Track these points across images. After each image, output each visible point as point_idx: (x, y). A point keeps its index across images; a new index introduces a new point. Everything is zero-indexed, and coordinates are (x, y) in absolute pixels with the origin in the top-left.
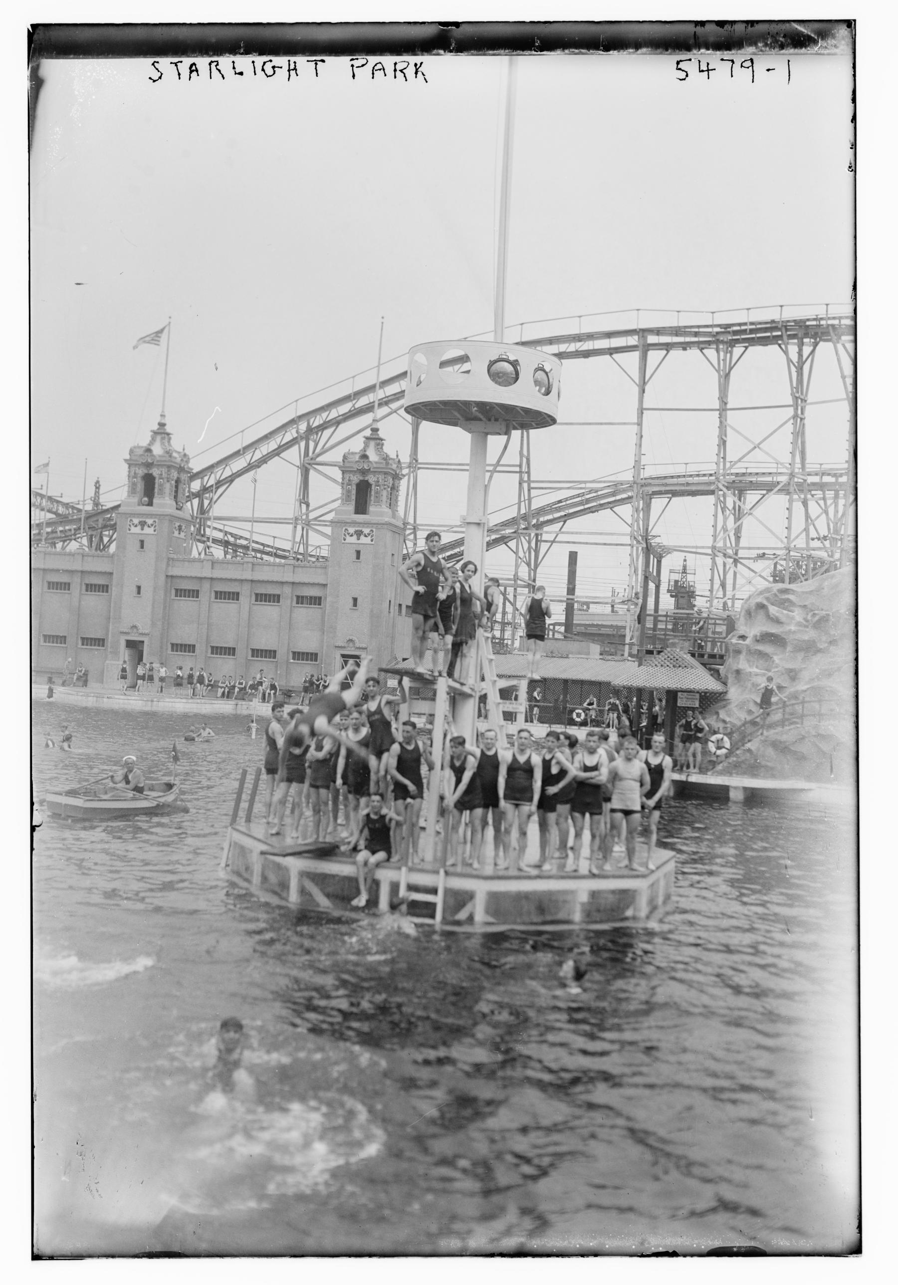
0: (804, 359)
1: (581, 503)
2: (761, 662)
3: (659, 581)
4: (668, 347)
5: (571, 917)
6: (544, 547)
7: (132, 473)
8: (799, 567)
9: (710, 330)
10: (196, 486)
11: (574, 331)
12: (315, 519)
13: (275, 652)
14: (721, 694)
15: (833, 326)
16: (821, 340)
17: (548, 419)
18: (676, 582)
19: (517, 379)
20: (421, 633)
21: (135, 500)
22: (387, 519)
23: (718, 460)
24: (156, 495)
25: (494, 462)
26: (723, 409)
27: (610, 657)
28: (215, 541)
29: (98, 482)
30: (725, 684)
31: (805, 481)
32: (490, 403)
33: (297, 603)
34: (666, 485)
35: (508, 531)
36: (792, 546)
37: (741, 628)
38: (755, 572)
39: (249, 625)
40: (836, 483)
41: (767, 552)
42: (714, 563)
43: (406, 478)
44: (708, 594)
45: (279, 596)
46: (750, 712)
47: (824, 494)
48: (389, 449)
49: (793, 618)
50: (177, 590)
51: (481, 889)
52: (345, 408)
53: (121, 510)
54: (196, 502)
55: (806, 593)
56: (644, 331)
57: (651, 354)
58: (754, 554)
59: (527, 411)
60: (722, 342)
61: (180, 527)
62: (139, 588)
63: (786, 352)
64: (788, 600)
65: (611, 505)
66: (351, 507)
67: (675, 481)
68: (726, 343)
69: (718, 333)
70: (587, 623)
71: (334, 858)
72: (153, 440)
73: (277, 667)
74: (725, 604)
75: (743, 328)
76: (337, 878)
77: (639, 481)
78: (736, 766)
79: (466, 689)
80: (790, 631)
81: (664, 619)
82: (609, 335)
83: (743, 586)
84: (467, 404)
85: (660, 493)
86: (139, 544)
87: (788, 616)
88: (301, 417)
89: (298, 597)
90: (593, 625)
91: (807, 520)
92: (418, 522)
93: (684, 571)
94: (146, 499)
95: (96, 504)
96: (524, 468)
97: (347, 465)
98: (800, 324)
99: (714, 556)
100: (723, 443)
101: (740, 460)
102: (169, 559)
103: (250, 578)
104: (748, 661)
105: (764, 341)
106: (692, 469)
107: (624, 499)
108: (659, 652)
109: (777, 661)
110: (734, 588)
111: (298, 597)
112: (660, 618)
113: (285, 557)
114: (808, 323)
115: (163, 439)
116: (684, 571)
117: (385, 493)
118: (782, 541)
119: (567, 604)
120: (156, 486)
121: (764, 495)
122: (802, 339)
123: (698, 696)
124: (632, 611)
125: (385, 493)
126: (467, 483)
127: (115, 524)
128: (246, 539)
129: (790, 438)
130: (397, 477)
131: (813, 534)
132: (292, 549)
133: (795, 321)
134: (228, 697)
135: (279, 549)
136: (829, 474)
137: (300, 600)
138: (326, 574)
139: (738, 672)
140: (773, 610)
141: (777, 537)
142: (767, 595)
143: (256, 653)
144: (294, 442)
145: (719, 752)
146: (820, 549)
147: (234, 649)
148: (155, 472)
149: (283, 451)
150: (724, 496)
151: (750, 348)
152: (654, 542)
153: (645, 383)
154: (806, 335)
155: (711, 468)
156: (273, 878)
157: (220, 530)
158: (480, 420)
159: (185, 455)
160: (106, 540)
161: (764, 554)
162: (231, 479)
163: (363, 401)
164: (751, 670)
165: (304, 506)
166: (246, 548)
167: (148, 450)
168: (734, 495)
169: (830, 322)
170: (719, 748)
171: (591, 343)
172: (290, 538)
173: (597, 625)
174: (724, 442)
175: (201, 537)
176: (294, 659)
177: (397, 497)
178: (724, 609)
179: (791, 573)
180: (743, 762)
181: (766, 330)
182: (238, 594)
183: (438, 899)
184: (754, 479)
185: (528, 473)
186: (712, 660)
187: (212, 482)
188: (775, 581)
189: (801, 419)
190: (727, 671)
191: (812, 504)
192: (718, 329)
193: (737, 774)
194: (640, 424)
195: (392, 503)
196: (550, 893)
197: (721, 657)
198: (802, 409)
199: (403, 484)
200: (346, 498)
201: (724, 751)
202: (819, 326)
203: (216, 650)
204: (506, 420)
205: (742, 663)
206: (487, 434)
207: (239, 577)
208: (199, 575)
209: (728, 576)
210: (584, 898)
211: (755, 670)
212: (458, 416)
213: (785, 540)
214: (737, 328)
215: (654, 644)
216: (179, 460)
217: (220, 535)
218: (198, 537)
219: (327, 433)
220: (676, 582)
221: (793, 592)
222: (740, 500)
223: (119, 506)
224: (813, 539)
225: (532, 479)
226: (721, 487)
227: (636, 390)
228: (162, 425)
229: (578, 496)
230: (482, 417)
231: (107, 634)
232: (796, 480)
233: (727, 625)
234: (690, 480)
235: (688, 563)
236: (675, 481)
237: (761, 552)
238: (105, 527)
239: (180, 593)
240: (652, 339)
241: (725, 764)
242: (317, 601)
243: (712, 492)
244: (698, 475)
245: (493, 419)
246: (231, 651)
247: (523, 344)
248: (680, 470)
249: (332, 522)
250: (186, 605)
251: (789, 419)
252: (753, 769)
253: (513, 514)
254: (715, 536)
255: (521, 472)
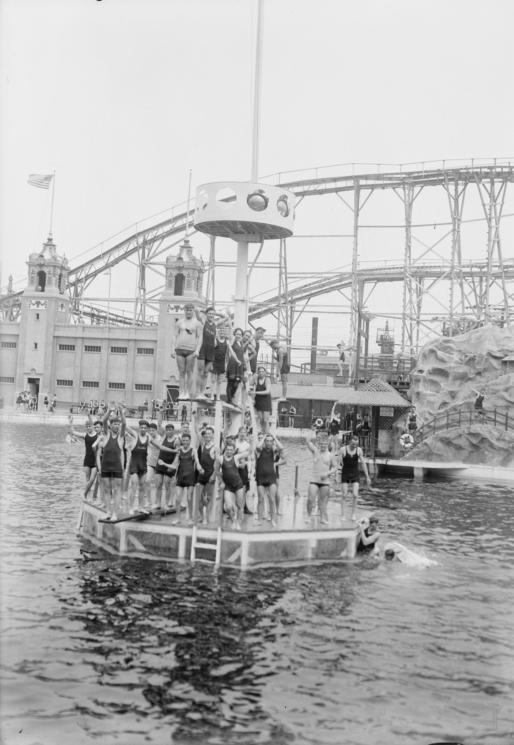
0: (459, 193)
1: (320, 287)
2: (433, 387)
3: (368, 336)
4: (373, 187)
5: (305, 557)
6: (296, 315)
7: (31, 271)
8: (459, 326)
9: (399, 176)
10: (72, 278)
11: (313, 177)
12: (150, 299)
13: (124, 384)
14: (408, 407)
15: (477, 173)
16: (469, 182)
17: (288, 232)
18: (382, 336)
19: (266, 206)
20: (202, 372)
21: (33, 288)
22: (195, 299)
23: (406, 258)
24: (46, 284)
25: (253, 261)
26: (408, 226)
27: (339, 385)
28: (85, 314)
29: (11, 277)
30: (410, 401)
31: (461, 271)
32: (249, 222)
33: (138, 353)
34: (373, 274)
35: (273, 305)
36: (454, 312)
37: (420, 366)
38: (431, 329)
39: (107, 368)
40: (481, 272)
41: (438, 316)
42: (404, 324)
43: (207, 272)
44: (401, 343)
45: (126, 348)
46: (426, 419)
47: (473, 279)
48: (196, 254)
49: (453, 359)
50: (60, 346)
51: (245, 540)
52: (168, 228)
53: (24, 294)
54: (72, 289)
55: (461, 342)
56: (357, 177)
57: (362, 191)
58: (430, 317)
59: (274, 227)
60: (407, 183)
61: (62, 306)
62: (36, 344)
63: (447, 190)
64: (450, 347)
65: (338, 288)
66: (172, 291)
67: (378, 272)
68: (410, 184)
69: (404, 178)
70: (326, 363)
71: (149, 521)
72: (45, 249)
73: (125, 394)
74: (412, 350)
75: (420, 174)
76: (151, 535)
77: (356, 272)
78: (417, 454)
79: (237, 409)
80: (451, 367)
81: (371, 360)
82: (335, 180)
83: (423, 338)
84: (234, 223)
85: (369, 280)
86: (36, 316)
87: (449, 357)
88: (139, 234)
89: (138, 349)
90: (330, 364)
91: (462, 296)
92: (215, 300)
93: (387, 329)
94: (40, 287)
95: (10, 291)
96: (283, 265)
97: (169, 264)
98: (456, 172)
99: (404, 319)
100: (408, 248)
101: (419, 259)
102: (55, 325)
103: (107, 337)
104: (425, 386)
105: (433, 183)
106: (389, 264)
107: (346, 284)
108: (368, 381)
109: (443, 386)
110: (417, 340)
111: (138, 349)
112: (368, 360)
113: (130, 324)
114: (461, 171)
115: (51, 249)
116: (387, 329)
117: (193, 282)
118: (447, 309)
119: (312, 351)
120: (47, 279)
121: (435, 280)
122: (457, 181)
123: (393, 409)
124: (353, 355)
125: (193, 282)
126: (235, 274)
127: (21, 304)
128: (106, 312)
129: (451, 244)
130: (201, 271)
131: (467, 305)
132: (135, 318)
133: (452, 170)
134: (94, 414)
135: (127, 318)
136: (476, 267)
137: (140, 351)
138: (156, 334)
139: (418, 393)
140: (440, 353)
141: (444, 307)
142: (436, 344)
143: (112, 385)
144: (135, 250)
145: (407, 445)
146: (471, 314)
147: (98, 383)
148: (46, 270)
149: (129, 255)
150: (410, 281)
151: (425, 187)
152: (364, 311)
153: (358, 210)
154: (460, 179)
155: (402, 264)
156: (110, 534)
157: (89, 307)
158: (243, 233)
159: (65, 259)
160: (15, 314)
161: (437, 318)
162: (95, 274)
163: (179, 223)
164: (426, 392)
165: (142, 291)
166: (105, 318)
167: (41, 256)
168: (417, 280)
169: (475, 170)
170: (406, 443)
171: (324, 185)
172: (133, 311)
173: (333, 364)
174: (410, 247)
175: (76, 311)
176: (136, 389)
177: (201, 284)
178: (411, 353)
179: (455, 330)
180: (422, 451)
181: (434, 176)
182: (100, 347)
183: (217, 548)
184: (429, 270)
185: (285, 268)
186: (402, 386)
187: (83, 276)
188: (444, 335)
189: (458, 232)
190: (411, 393)
191: (466, 286)
192: (404, 176)
193: (419, 459)
194: (356, 236)
195: (198, 288)
196: (291, 542)
197: (408, 384)
198: (458, 226)
199: (205, 276)
200: (169, 285)
201: (410, 445)
202: (468, 173)
203: (86, 384)
204: (260, 233)
205: (421, 388)
206: (248, 242)
207: (100, 337)
208: (75, 336)
209: (413, 332)
210: (313, 544)
211: (429, 392)
212: (229, 230)
213: (449, 309)
214: (417, 175)
215: (365, 376)
216: (61, 262)
217: (88, 310)
218: (74, 311)
219: (156, 244)
220: (382, 336)
221: (453, 342)
222: (420, 284)
223: (23, 292)
224: (467, 308)
225: (288, 272)
226: (408, 275)
227: (353, 214)
228: (50, 240)
229: (317, 282)
230: (244, 231)
231: (16, 375)
232: (455, 270)
233: (411, 363)
234: (388, 271)
235: (389, 324)
236: (378, 272)
237: (435, 316)
238: (14, 305)
239: (62, 347)
240: (362, 182)
241: (411, 453)
242: (150, 351)
243: (402, 279)
244: (393, 268)
245: (251, 232)
246: (96, 384)
247: (281, 186)
248: (382, 265)
249: (160, 300)
250: (66, 355)
251: (450, 232)
252: (429, 456)
253: (276, 294)
254: (404, 307)
255: (280, 267)
